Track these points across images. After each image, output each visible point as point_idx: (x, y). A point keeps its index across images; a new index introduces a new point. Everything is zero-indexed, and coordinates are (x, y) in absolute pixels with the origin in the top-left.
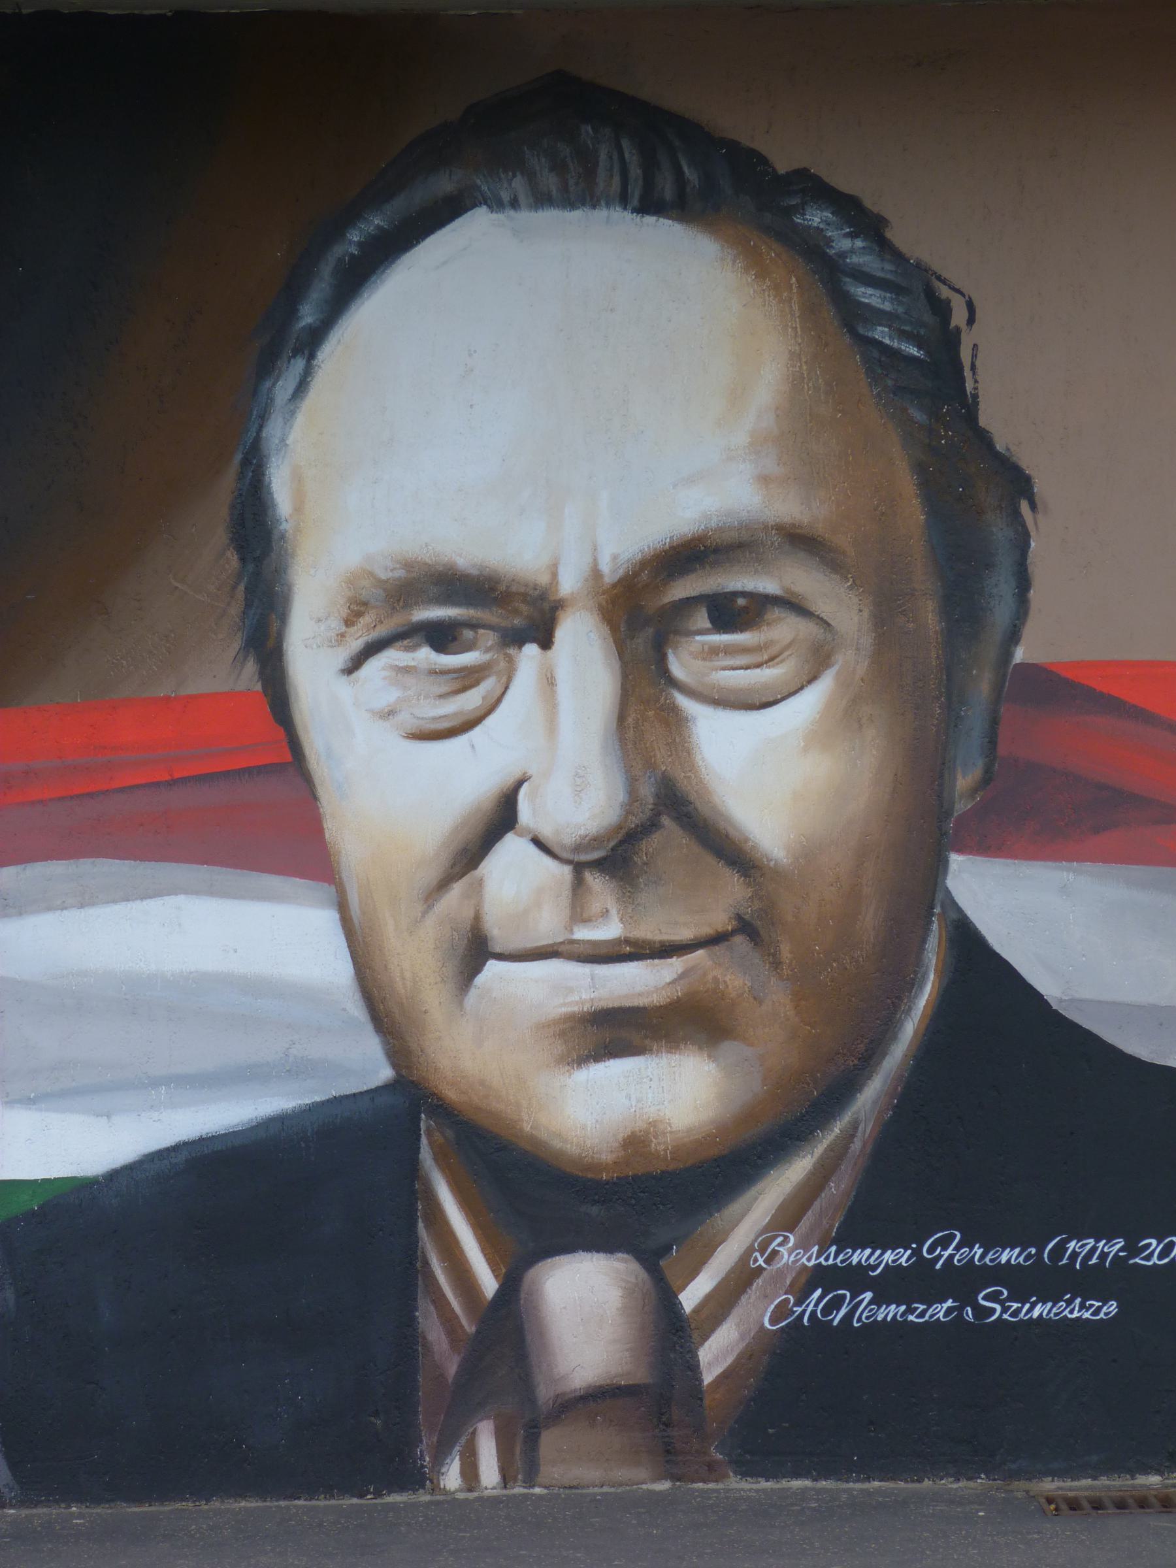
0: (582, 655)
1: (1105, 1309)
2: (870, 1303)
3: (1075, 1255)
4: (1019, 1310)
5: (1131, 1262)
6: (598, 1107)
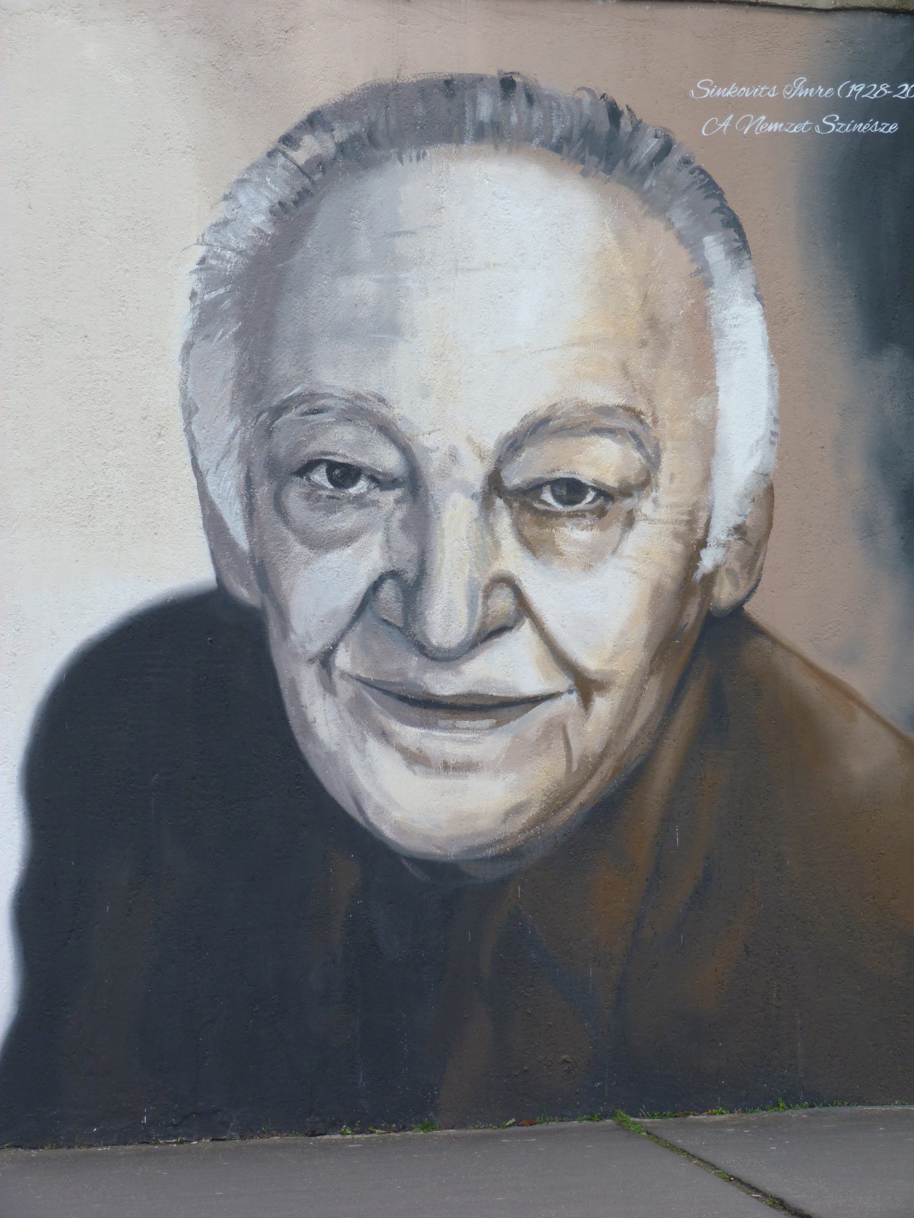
1: (891, 128)
2: (763, 123)
3: (854, 93)
4: (844, 128)
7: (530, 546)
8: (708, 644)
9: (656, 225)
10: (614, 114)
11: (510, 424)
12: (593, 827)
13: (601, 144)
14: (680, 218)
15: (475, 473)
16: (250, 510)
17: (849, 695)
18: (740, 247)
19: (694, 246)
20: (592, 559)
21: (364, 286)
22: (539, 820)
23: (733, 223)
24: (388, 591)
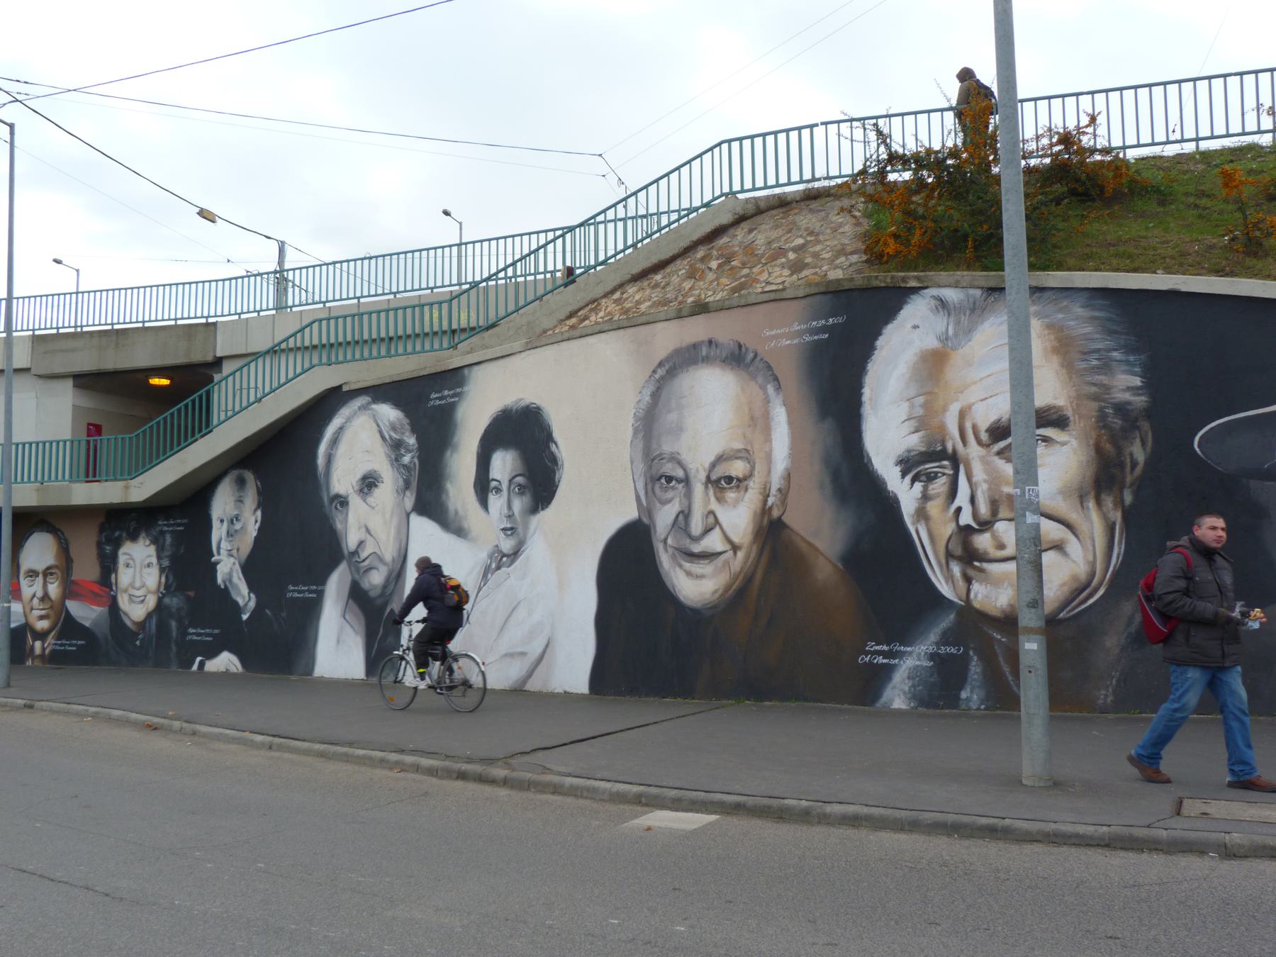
0: (40, 579)
5: (243, 595)
7: (720, 500)
8: (771, 530)
9: (753, 383)
10: (740, 346)
11: (712, 458)
12: (738, 597)
13: (737, 358)
14: (760, 380)
15: (702, 476)
16: (646, 493)
17: (817, 549)
18: (778, 388)
19: (763, 388)
20: (736, 503)
21: (672, 417)
22: (722, 595)
23: (776, 379)
24: (681, 517)
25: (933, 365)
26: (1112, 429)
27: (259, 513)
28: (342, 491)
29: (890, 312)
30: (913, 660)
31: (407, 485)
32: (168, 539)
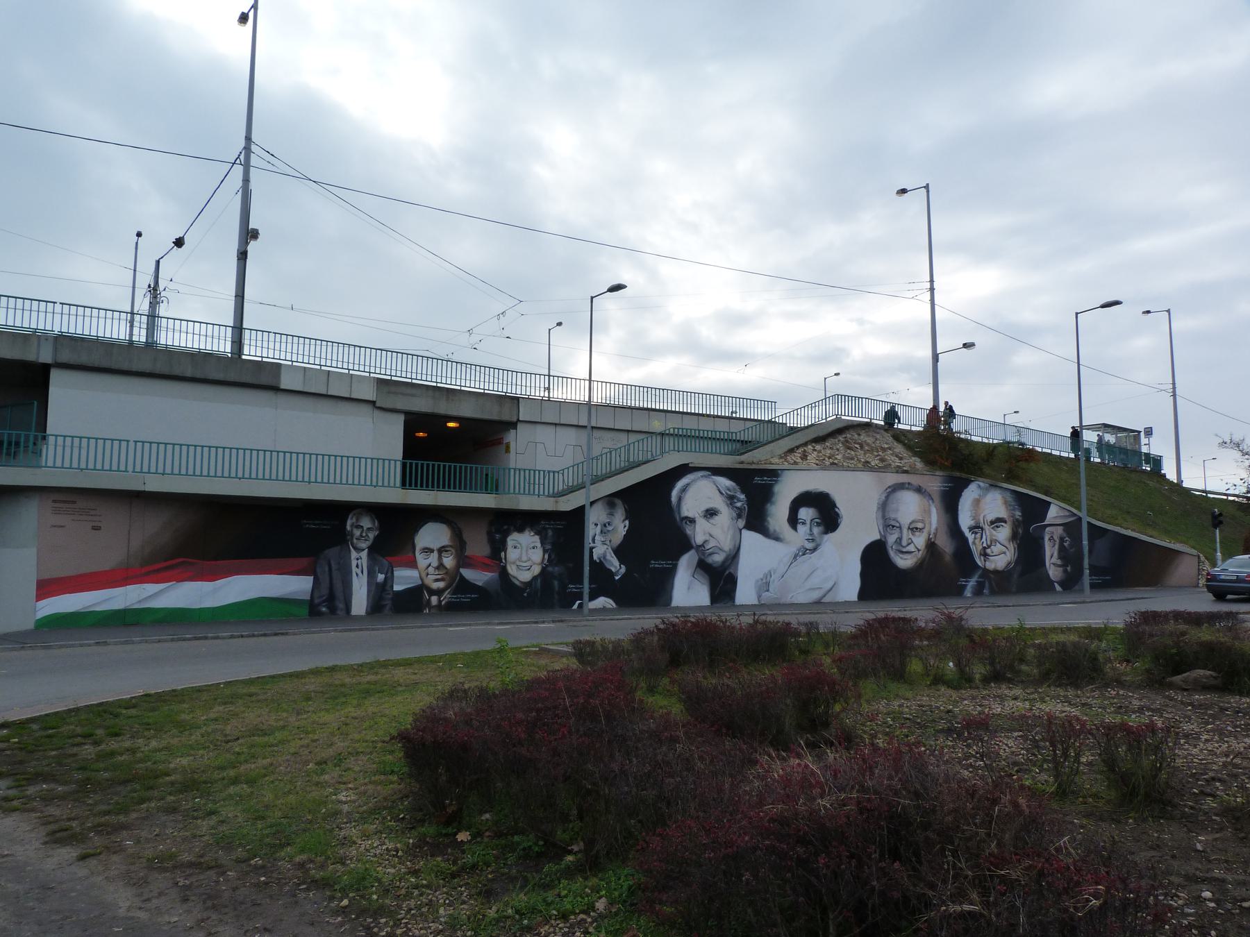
0: (436, 554)
6: (435, 586)
8: (931, 546)
12: (920, 566)
13: (919, 490)
25: (977, 502)
26: (1016, 525)
27: (627, 522)
28: (690, 515)
29: (966, 486)
30: (972, 582)
31: (739, 516)
32: (550, 533)
